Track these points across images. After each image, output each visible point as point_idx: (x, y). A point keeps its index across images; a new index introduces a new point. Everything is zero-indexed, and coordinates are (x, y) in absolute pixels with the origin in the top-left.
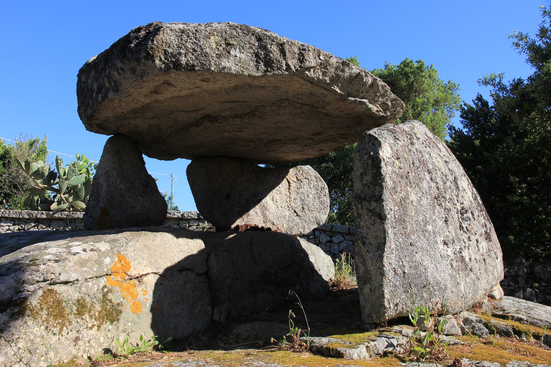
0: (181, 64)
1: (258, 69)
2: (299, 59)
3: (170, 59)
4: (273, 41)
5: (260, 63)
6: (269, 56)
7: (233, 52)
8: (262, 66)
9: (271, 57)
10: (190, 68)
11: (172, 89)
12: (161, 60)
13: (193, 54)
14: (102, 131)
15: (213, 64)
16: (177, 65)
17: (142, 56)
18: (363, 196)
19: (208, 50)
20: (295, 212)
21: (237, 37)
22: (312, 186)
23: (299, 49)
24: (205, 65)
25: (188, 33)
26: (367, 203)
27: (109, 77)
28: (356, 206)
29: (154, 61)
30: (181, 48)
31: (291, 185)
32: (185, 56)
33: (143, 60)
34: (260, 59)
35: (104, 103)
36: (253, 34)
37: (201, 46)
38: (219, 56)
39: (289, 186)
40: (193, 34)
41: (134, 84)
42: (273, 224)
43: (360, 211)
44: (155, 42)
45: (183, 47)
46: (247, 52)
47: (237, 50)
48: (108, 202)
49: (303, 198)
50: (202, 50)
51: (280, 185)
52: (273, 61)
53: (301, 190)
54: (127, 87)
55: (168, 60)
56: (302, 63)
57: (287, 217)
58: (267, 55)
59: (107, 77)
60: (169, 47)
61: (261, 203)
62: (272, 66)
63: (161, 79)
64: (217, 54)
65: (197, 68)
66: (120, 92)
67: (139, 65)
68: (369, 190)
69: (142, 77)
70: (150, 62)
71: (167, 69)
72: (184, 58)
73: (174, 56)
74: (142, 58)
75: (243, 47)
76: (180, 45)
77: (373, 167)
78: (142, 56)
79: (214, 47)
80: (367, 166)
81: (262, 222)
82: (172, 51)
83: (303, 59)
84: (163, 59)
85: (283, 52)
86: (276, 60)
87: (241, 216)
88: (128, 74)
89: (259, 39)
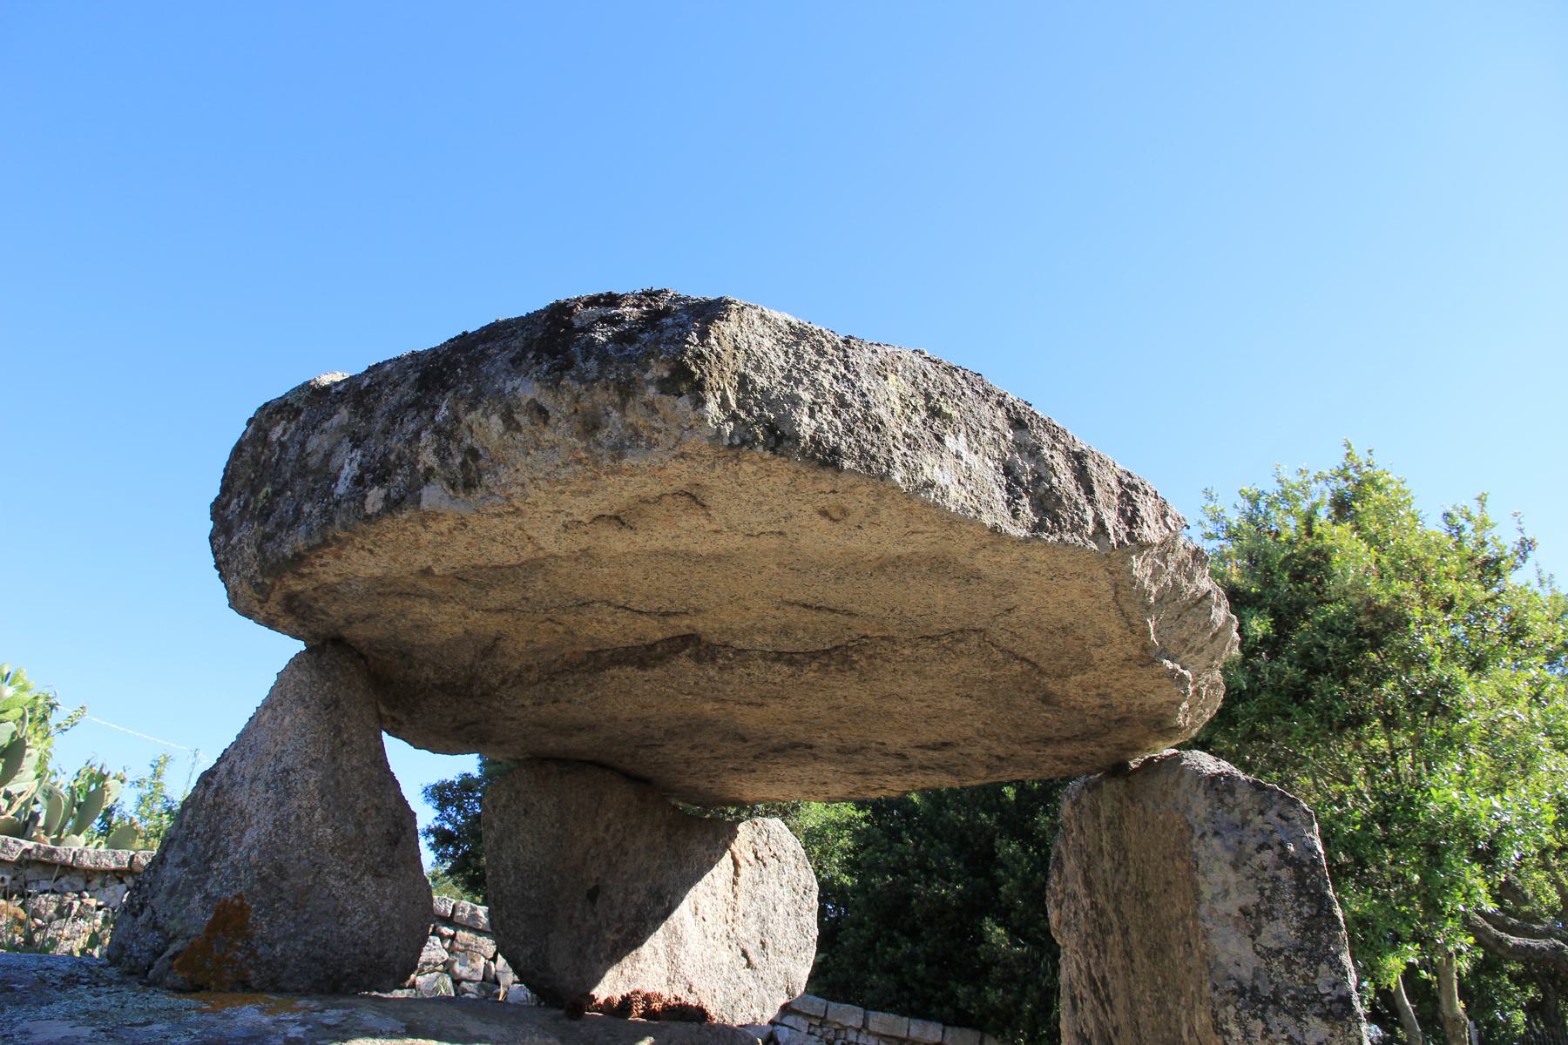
0: (796, 438)
2: (1122, 513)
5: (1021, 497)
6: (1049, 482)
7: (949, 440)
9: (1052, 487)
10: (828, 459)
11: (696, 520)
12: (724, 404)
14: (288, 621)
15: (898, 464)
16: (779, 438)
18: (1266, 991)
19: (882, 412)
20: (745, 954)
22: (785, 878)
24: (873, 458)
25: (821, 343)
26: (1286, 1020)
27: (446, 434)
28: (1240, 1022)
29: (700, 402)
30: (798, 382)
31: (742, 871)
32: (811, 410)
33: (652, 390)
34: (1020, 484)
35: (386, 522)
36: (1000, 404)
39: (736, 873)
40: (836, 348)
41: (564, 474)
42: (690, 991)
45: (805, 380)
46: (985, 454)
47: (962, 436)
48: (257, 887)
49: (764, 913)
50: (867, 405)
51: (715, 870)
52: (1059, 499)
53: (761, 890)
54: (524, 477)
55: (749, 413)
57: (725, 969)
59: (438, 431)
60: (757, 369)
61: (669, 921)
63: (681, 474)
65: (847, 464)
66: (480, 493)
67: (622, 407)
68: (1292, 972)
69: (619, 451)
70: (684, 403)
71: (742, 443)
72: (806, 419)
73: (773, 405)
74: (650, 382)
75: (977, 434)
77: (1299, 895)
78: (648, 376)
79: (898, 409)
80: (1275, 890)
81: (664, 980)
82: (766, 384)
86: (1070, 499)
87: (619, 960)
88: (560, 433)
89: (1018, 424)
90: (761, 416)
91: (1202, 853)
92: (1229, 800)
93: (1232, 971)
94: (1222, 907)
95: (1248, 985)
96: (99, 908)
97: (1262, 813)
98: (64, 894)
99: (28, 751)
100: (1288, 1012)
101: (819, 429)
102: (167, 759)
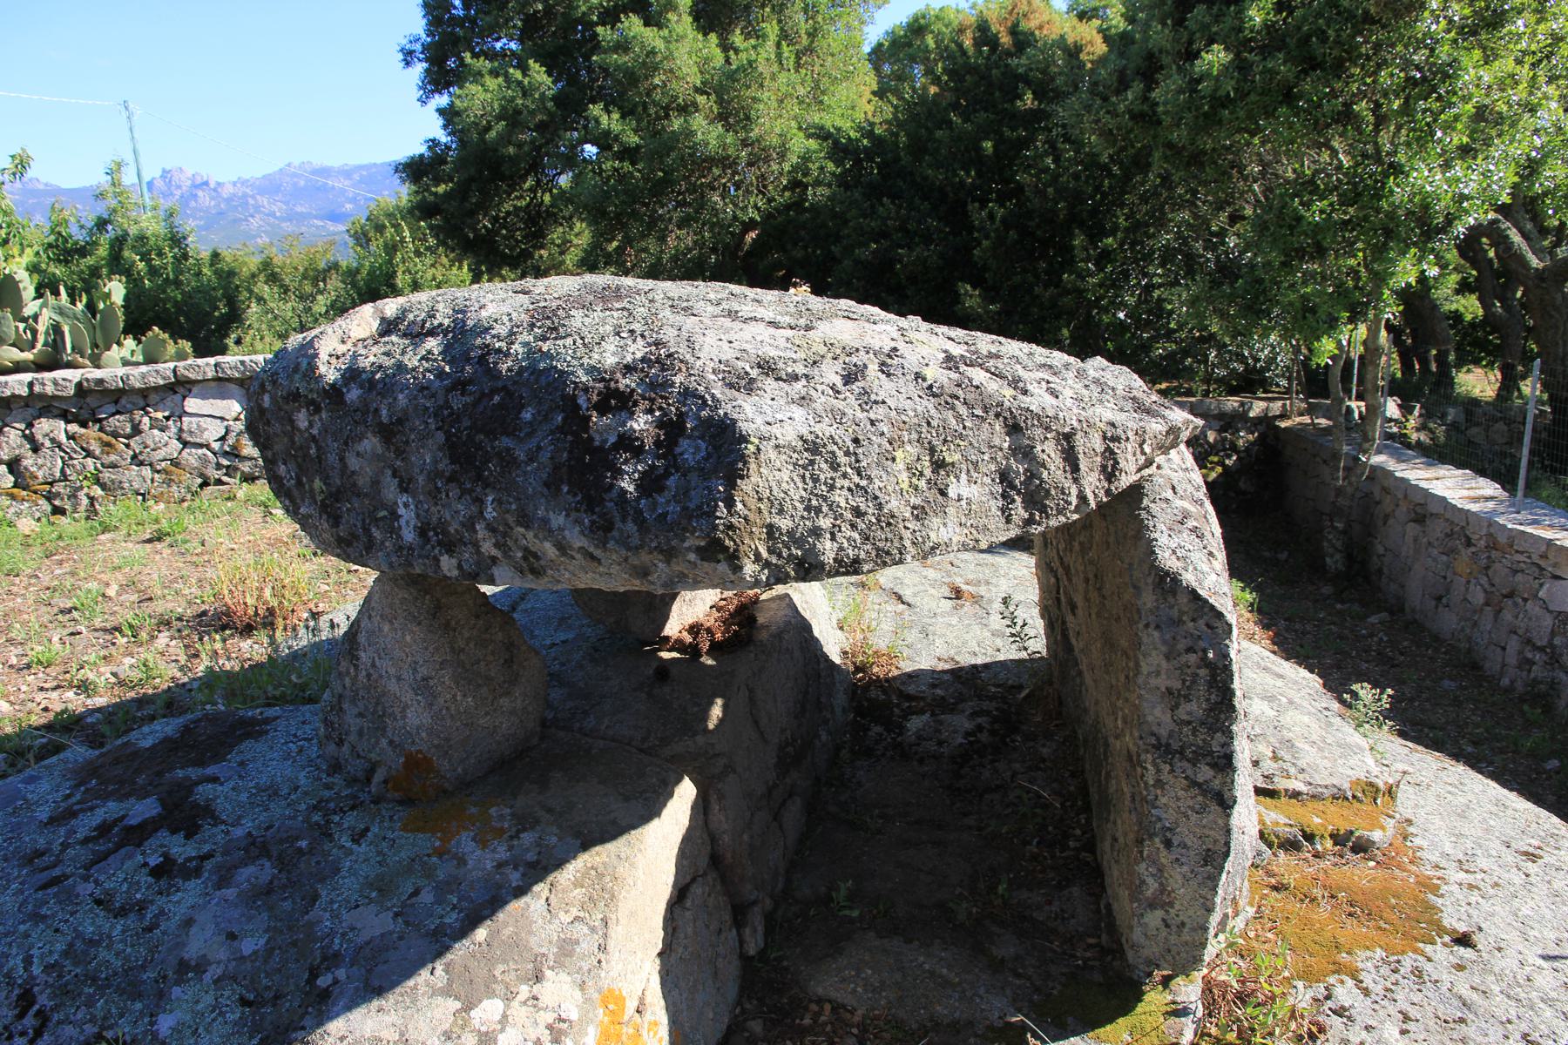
0: (823, 564)
1: (1008, 521)
3: (785, 553)
4: (1048, 429)
8: (1019, 512)
9: (1042, 481)
13: (853, 526)
15: (907, 543)
17: (686, 544)
18: (1175, 746)
21: (961, 436)
23: (1105, 438)
24: (888, 553)
25: (833, 453)
26: (1185, 764)
30: (818, 510)
34: (1013, 487)
36: (997, 415)
37: (876, 498)
38: (920, 513)
40: (847, 454)
43: (1165, 776)
44: (739, 506)
45: (825, 509)
47: (964, 477)
52: (1048, 492)
55: (780, 556)
56: (1110, 482)
58: (1031, 475)
60: (781, 512)
62: (1045, 506)
64: (914, 508)
72: (828, 544)
73: (800, 542)
74: (689, 549)
76: (814, 502)
78: (686, 544)
80: (1194, 682)
82: (790, 524)
83: (1114, 467)
84: (765, 554)
85: (1071, 459)
89: (1014, 429)
90: (790, 555)
91: (1145, 639)
92: (1171, 600)
93: (1154, 728)
94: (1154, 682)
95: (1164, 741)
96: (167, 418)
97: (1193, 620)
98: (131, 412)
99: (21, 286)
100: (1188, 761)
101: (841, 549)
102: (119, 165)
